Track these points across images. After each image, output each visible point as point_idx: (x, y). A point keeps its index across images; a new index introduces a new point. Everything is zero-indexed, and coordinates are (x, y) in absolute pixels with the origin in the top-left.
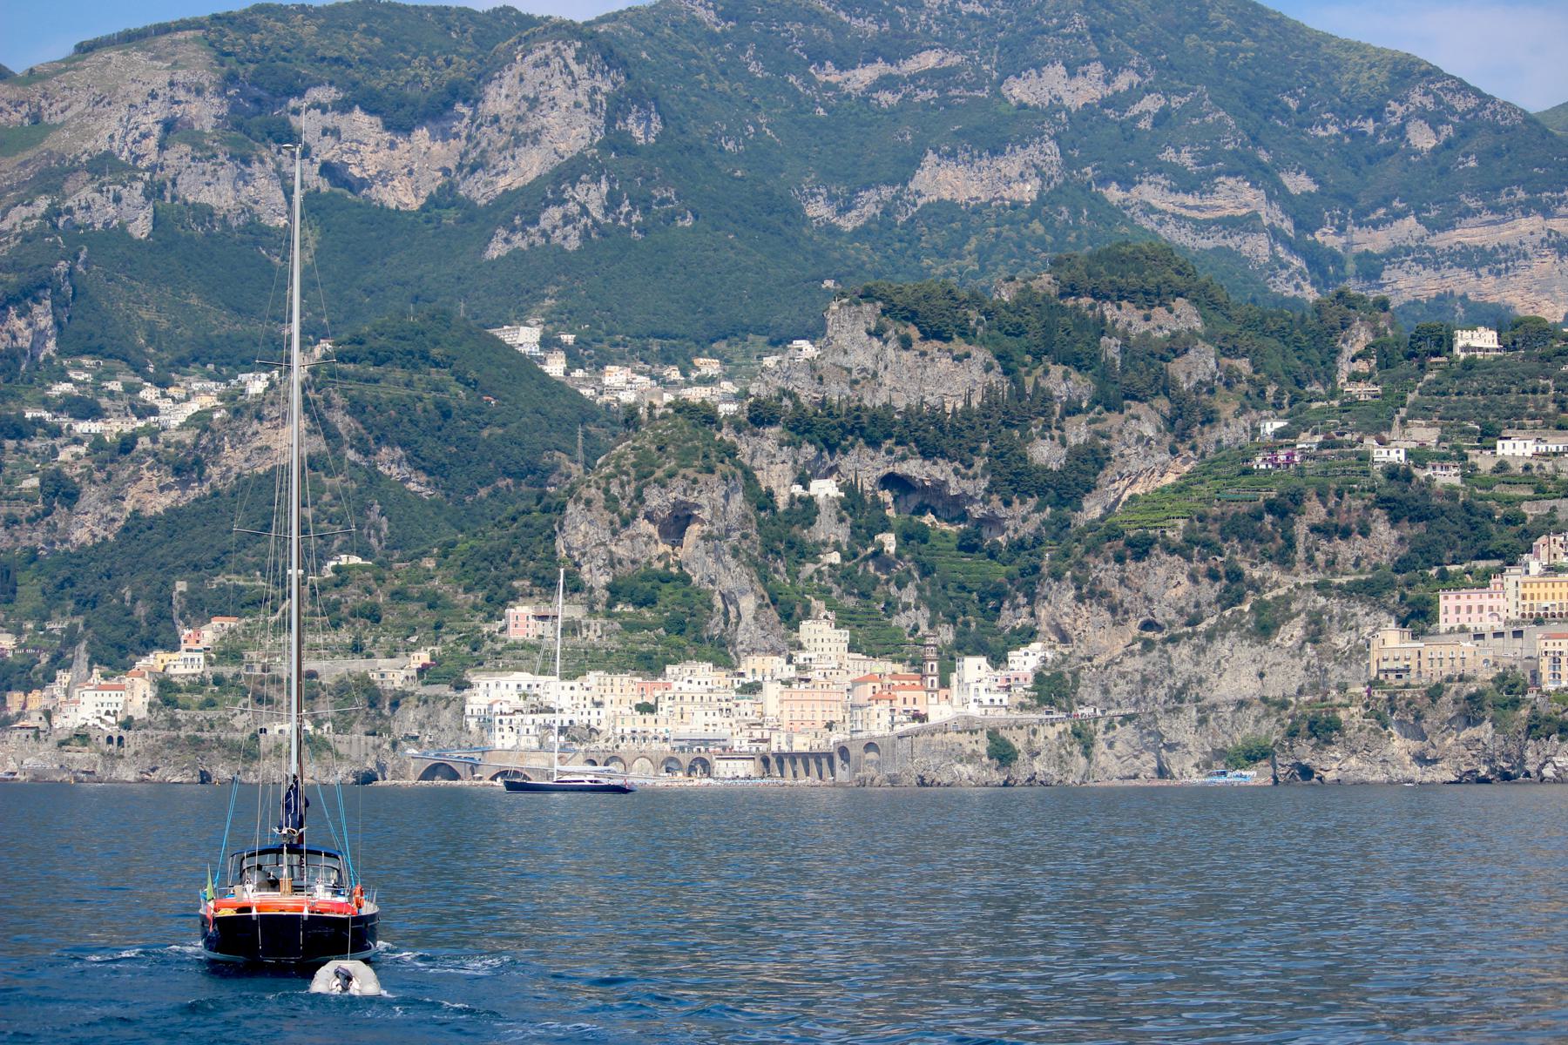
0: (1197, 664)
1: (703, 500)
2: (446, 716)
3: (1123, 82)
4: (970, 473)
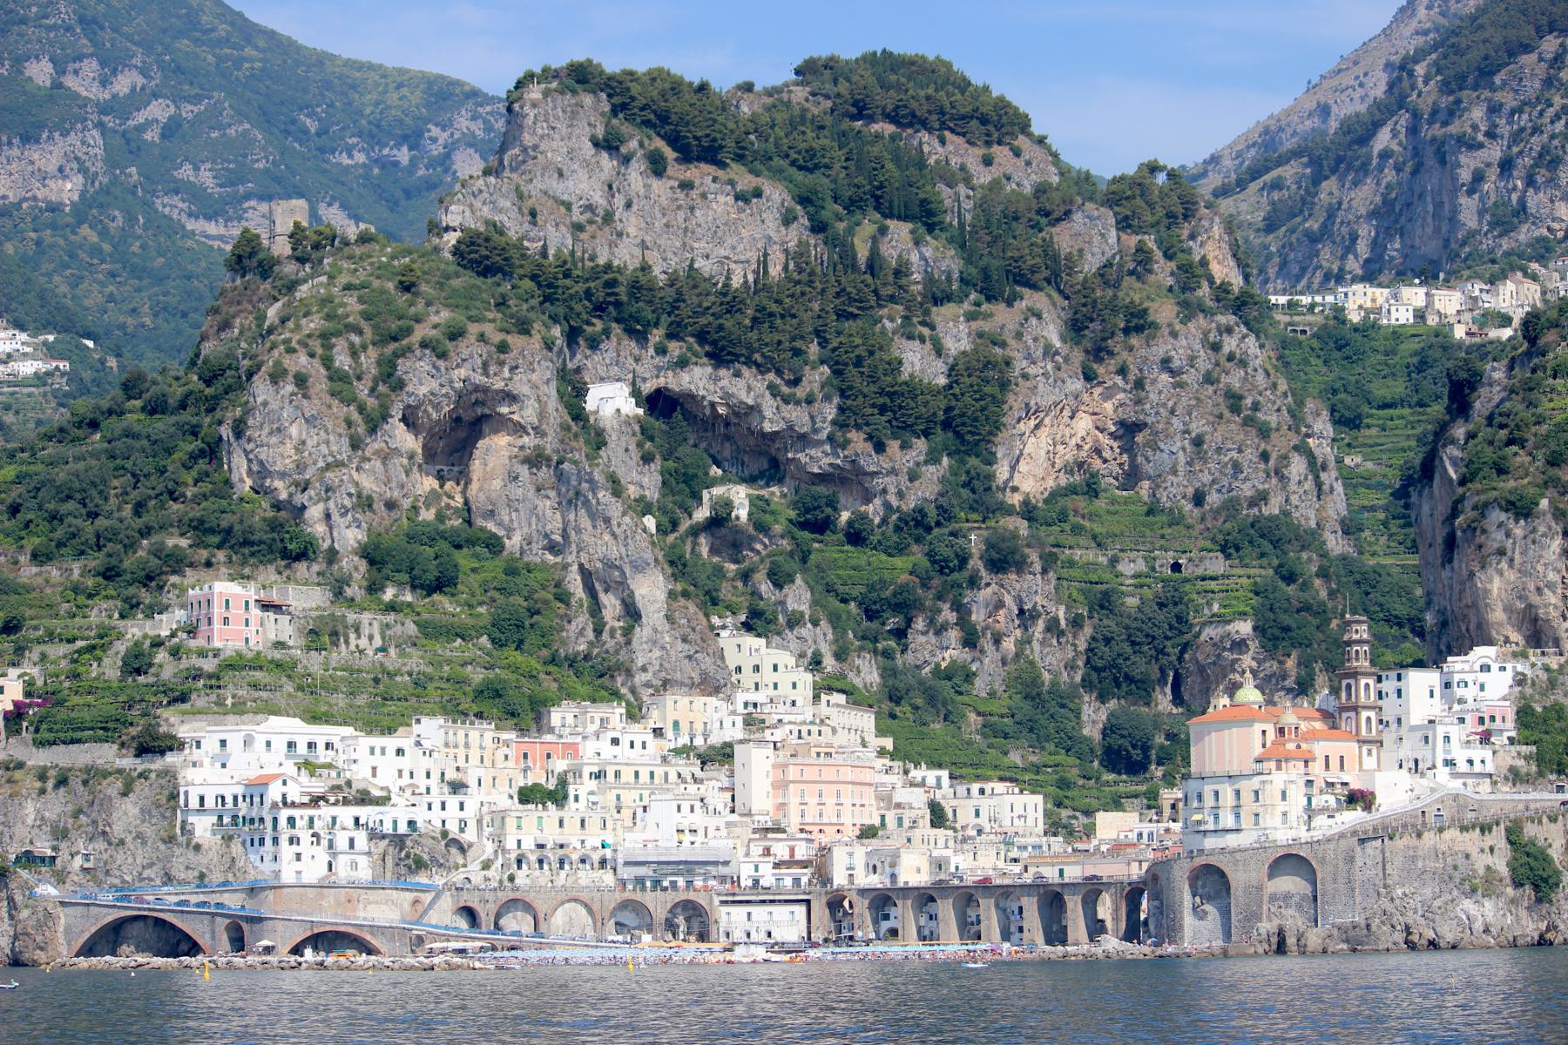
1: (520, 386)
2: (126, 814)
3: (123, 84)
4: (800, 392)
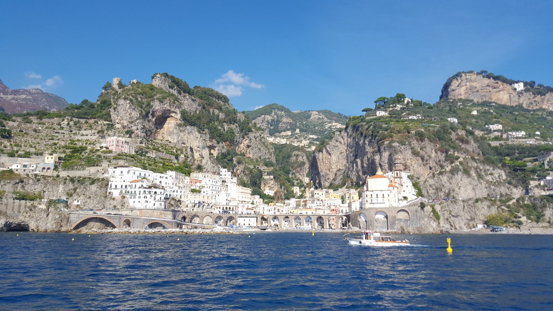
0: (451, 183)
4: (204, 132)
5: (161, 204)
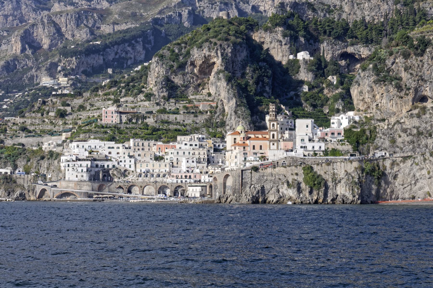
5: (82, 176)
